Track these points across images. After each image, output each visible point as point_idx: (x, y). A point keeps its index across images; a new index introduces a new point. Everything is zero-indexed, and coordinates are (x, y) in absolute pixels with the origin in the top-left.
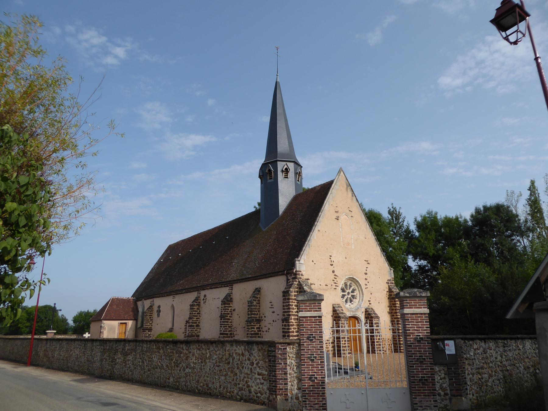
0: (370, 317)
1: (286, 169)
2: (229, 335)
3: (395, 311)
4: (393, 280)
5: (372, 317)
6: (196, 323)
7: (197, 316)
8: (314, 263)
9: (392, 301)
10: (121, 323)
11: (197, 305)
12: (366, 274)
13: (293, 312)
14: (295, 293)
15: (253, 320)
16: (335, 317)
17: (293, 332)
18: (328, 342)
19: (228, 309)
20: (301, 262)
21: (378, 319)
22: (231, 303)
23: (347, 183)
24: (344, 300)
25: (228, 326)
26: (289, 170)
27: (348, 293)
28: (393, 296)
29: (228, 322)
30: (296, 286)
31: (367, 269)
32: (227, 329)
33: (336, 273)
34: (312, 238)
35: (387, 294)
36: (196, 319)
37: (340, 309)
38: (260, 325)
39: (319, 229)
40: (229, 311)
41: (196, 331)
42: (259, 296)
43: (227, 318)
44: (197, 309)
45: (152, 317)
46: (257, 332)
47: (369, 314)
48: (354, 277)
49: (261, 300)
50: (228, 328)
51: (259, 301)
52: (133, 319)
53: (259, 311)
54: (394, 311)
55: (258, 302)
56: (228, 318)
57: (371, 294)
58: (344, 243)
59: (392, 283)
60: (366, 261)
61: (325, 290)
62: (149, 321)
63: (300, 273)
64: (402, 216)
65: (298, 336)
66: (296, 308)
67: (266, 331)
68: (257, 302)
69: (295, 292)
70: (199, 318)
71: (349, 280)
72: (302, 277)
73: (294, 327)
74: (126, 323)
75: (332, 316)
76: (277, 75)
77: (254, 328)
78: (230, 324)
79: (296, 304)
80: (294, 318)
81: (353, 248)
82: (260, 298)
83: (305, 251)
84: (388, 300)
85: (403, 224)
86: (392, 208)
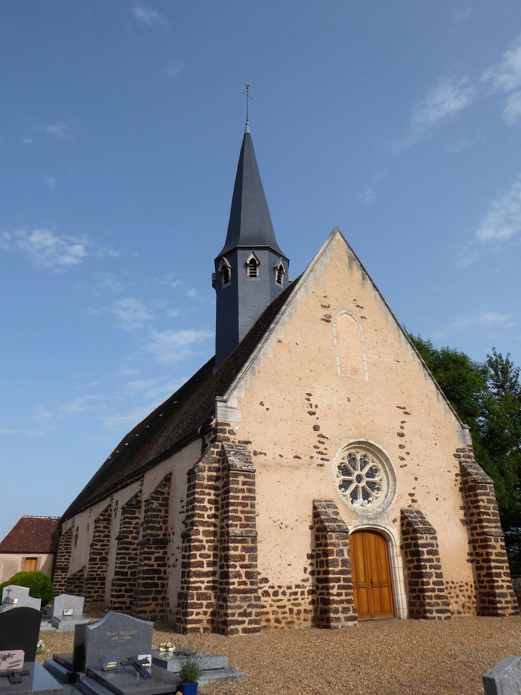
0: (411, 530)
1: (253, 261)
2: (129, 576)
3: (479, 518)
4: (470, 451)
5: (415, 531)
6: (102, 554)
7: (103, 541)
8: (264, 408)
9: (470, 496)
10: (27, 558)
11: (103, 520)
12: (401, 435)
13: (202, 516)
14: (210, 474)
15: (148, 540)
16: (318, 530)
17: (201, 564)
18: (299, 590)
19: (131, 523)
20: (229, 404)
21: (431, 536)
22: (137, 511)
23: (348, 253)
24: (348, 492)
25: (127, 557)
26: (257, 262)
27: (359, 478)
28: (470, 484)
29: (128, 549)
30: (215, 456)
31: (403, 425)
32: (126, 563)
33: (321, 431)
34: (261, 356)
35: (456, 480)
36: (102, 546)
37: (330, 511)
38: (165, 553)
39: (281, 337)
40: (132, 526)
41: (99, 570)
42: (166, 490)
43: (126, 540)
44: (104, 527)
45: (69, 547)
46: (156, 567)
47: (410, 524)
48: (370, 441)
49: (170, 499)
50: (127, 560)
51: (166, 499)
52: (48, 551)
53: (165, 522)
54: (475, 518)
55: (164, 502)
56: (130, 540)
57: (416, 479)
58: (343, 370)
59: (469, 457)
60: (400, 408)
61: (292, 467)
62: (64, 554)
63: (226, 427)
64: (513, 367)
65: (214, 574)
66: (211, 508)
67: (173, 566)
68: (160, 502)
69: (210, 470)
70: (107, 545)
71: (361, 448)
72: (232, 437)
73: (203, 552)
74: (36, 559)
75: (311, 528)
76: (246, 124)
77: (149, 559)
78: (133, 552)
79: (213, 497)
80: (204, 532)
81: (367, 379)
82: (168, 493)
83: (242, 382)
84: (460, 494)
85: (516, 382)
86: (494, 355)
